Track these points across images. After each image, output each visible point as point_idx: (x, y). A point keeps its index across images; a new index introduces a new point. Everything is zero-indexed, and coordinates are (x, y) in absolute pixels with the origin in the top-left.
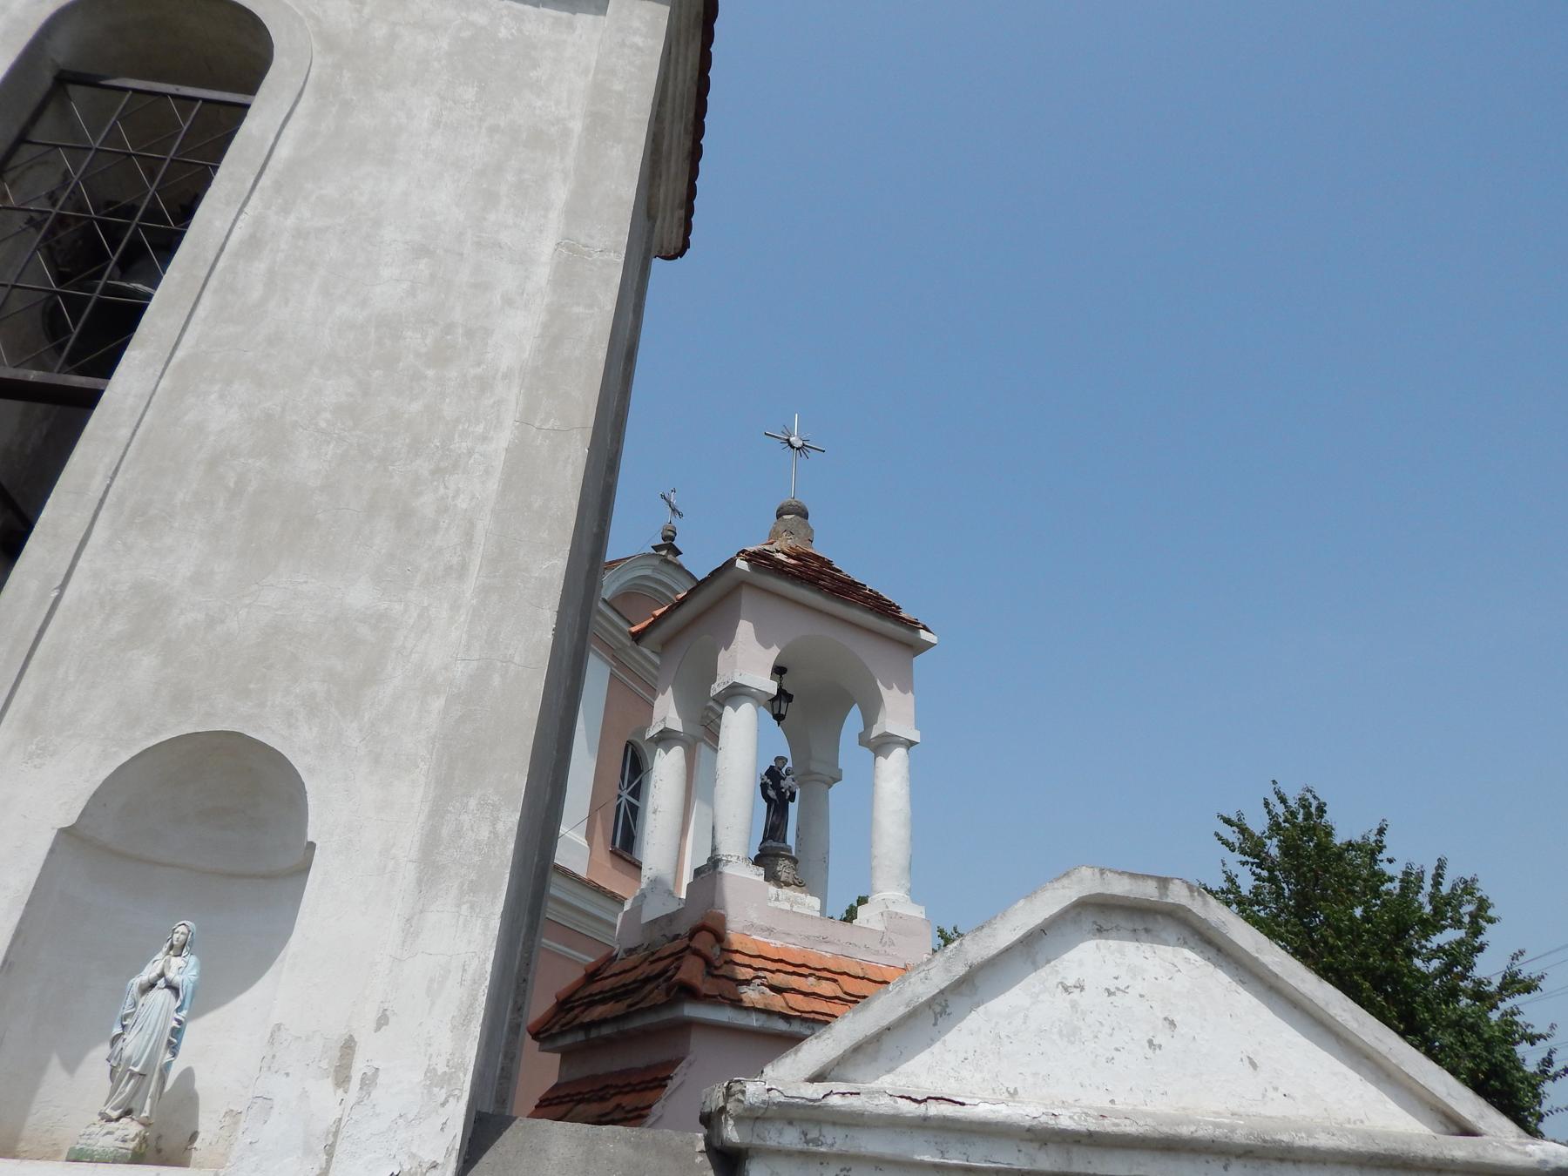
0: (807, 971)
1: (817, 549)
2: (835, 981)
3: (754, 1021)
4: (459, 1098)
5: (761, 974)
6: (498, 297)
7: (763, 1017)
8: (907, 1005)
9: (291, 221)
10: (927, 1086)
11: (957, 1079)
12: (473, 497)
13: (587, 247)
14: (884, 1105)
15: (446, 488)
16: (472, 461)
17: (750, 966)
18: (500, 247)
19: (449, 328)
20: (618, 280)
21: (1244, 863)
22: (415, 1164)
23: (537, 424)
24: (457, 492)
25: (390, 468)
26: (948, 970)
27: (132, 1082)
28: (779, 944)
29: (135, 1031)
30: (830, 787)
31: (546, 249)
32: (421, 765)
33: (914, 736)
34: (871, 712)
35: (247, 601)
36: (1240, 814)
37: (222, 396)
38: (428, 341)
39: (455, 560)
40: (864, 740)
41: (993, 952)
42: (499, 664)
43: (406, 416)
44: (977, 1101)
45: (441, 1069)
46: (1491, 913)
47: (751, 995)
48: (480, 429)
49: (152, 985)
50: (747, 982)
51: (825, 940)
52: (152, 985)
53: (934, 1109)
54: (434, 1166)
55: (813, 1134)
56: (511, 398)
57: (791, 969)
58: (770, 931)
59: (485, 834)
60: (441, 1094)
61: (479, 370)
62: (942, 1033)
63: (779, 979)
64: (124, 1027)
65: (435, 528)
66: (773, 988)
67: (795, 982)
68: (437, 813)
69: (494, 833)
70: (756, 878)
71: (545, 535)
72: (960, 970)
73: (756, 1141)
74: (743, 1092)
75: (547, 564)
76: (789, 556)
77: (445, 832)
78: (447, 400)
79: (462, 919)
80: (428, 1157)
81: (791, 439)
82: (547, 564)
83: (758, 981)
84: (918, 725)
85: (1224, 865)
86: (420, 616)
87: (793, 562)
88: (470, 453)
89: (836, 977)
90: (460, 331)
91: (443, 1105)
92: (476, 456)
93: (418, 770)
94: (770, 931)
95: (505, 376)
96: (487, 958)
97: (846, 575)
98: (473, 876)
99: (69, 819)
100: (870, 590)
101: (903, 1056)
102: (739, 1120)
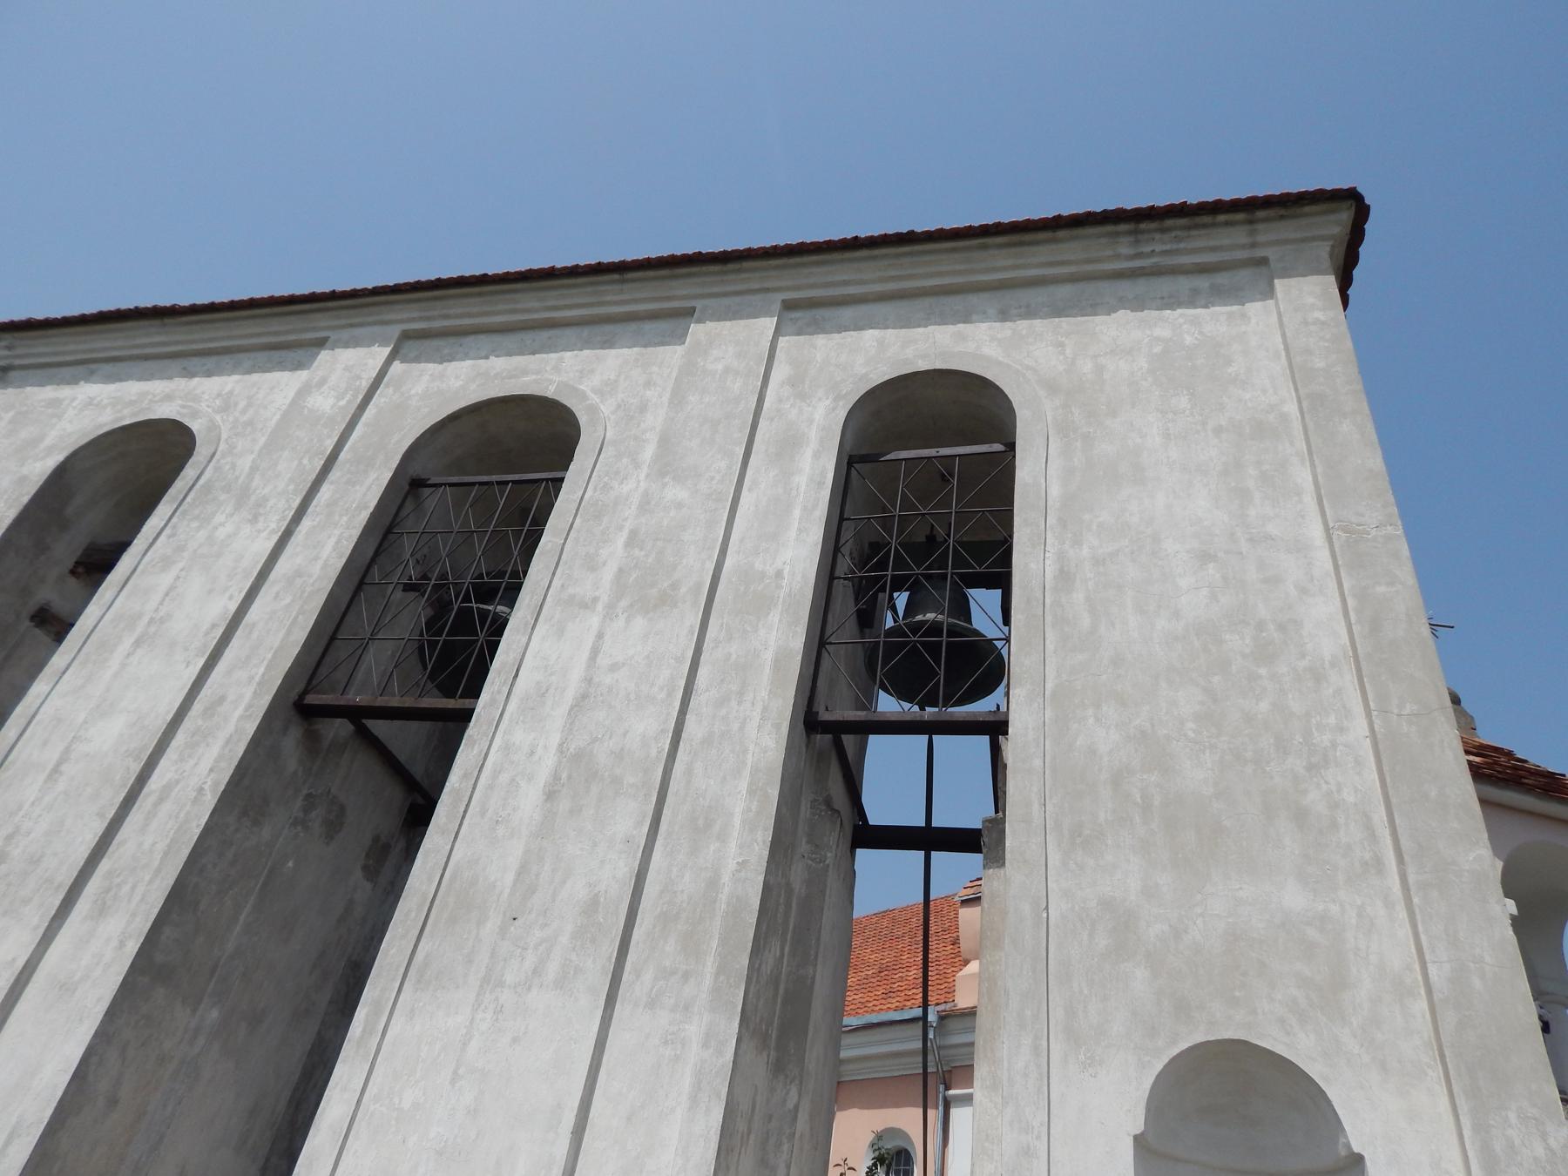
9: (1085, 551)
15: (1327, 783)
16: (1338, 754)
19: (1261, 626)
23: (1396, 711)
32: (1430, 1072)
35: (1199, 910)
37: (1097, 720)
38: (1247, 641)
39: (1367, 856)
42: (1472, 965)
48: (1332, 720)
59: (1540, 1151)
69: (1548, 1148)
77: (1498, 1146)
78: (1290, 696)
88: (1334, 745)
95: (1333, 665)
99: (1138, 1126)
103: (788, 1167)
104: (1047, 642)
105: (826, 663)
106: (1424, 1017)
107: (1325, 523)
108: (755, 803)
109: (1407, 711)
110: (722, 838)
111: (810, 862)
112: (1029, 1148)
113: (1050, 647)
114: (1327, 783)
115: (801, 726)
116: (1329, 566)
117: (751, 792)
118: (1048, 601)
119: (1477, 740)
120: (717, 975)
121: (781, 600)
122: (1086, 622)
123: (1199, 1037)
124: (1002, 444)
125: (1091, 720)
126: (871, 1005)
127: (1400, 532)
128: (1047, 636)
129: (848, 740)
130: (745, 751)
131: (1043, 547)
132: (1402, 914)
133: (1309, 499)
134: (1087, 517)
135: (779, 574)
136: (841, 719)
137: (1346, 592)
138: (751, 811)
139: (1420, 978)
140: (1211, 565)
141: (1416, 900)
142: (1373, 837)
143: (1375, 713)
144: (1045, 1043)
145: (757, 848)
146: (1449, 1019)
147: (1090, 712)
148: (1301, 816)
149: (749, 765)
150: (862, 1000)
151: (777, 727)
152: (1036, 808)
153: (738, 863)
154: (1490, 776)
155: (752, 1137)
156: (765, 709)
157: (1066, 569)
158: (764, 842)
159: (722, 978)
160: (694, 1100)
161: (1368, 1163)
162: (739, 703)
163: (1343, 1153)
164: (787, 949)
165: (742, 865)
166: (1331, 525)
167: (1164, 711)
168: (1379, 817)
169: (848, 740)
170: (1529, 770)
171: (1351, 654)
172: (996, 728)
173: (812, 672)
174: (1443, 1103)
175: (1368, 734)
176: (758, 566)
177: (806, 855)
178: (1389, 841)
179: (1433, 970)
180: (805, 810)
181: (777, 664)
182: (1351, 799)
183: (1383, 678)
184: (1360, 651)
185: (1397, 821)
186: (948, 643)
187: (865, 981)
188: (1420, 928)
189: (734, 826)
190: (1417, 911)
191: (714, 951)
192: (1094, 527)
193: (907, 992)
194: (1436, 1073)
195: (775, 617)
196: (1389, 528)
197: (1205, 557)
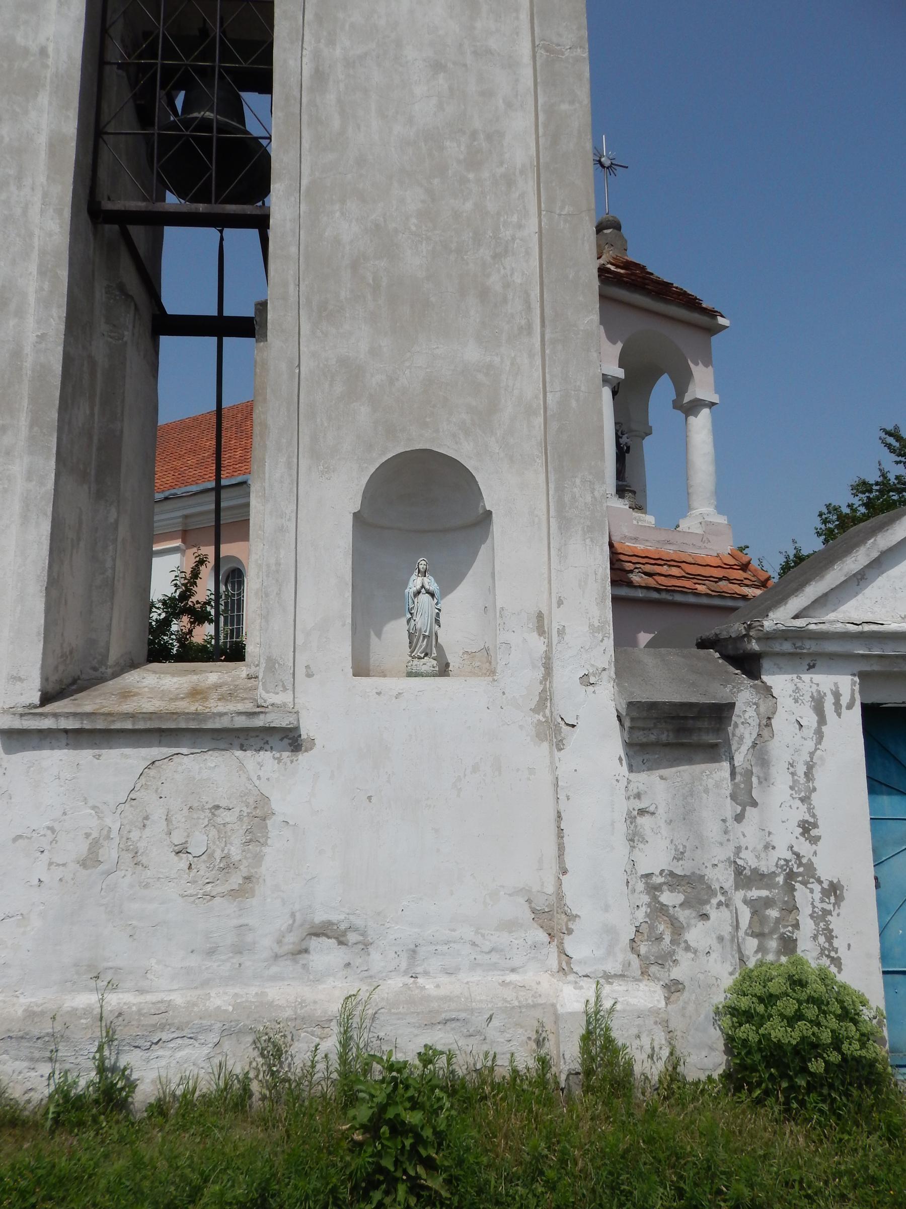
0: (663, 562)
1: (632, 256)
2: (679, 567)
3: (640, 594)
4: (609, 638)
5: (638, 566)
6: (501, 101)
7: (645, 591)
8: (846, 576)
9: (338, 52)
10: (857, 617)
11: (872, 613)
12: (523, 274)
13: (559, 45)
14: (839, 627)
15: (504, 268)
16: (515, 246)
17: (630, 562)
18: (491, 53)
19: (474, 135)
20: (587, 75)
21: (897, 463)
22: (595, 669)
23: (558, 212)
24: (513, 270)
25: (465, 257)
26: (868, 555)
27: (426, 640)
28: (642, 547)
29: (419, 616)
30: (643, 439)
31: (524, 49)
32: (537, 460)
33: (715, 398)
34: (682, 381)
35: (407, 364)
36: (896, 428)
37: (342, 214)
38: (463, 148)
39: (523, 322)
40: (678, 405)
41: (894, 543)
42: (573, 393)
43: (465, 214)
44: (890, 623)
45: (596, 624)
46: (886, 470)
47: (636, 578)
48: (515, 219)
49: (419, 592)
50: (631, 571)
51: (669, 543)
52: (419, 592)
53: (867, 628)
54: (604, 669)
55: (799, 644)
56: (527, 186)
57: (654, 562)
58: (636, 539)
59: (589, 499)
60: (600, 636)
61: (502, 170)
62: (862, 589)
63: (648, 568)
64: (411, 614)
65: (505, 300)
66: (646, 574)
67: (657, 569)
68: (559, 489)
69: (594, 497)
70: (624, 507)
71: (581, 298)
72: (875, 554)
73: (768, 649)
74: (762, 626)
75: (587, 319)
76: (617, 266)
77: (567, 499)
78: (488, 197)
79: (588, 548)
80: (601, 666)
81: (603, 160)
82: (587, 319)
83: (637, 570)
84: (717, 391)
85: (880, 465)
86: (512, 364)
87: (622, 271)
88: (513, 239)
89: (679, 564)
90: (482, 136)
91: (602, 641)
92: (518, 241)
93: (536, 464)
94: (636, 539)
95: (522, 172)
96: (607, 567)
97: (657, 277)
98: (588, 523)
99: (357, 507)
100: (677, 288)
101: (841, 602)
102: (758, 639)
103: (114, 560)
104: (303, 141)
105: (106, 156)
106: (540, 427)
107: (533, 41)
108: (47, 283)
109: (564, 212)
110: (20, 313)
111: (110, 340)
112: (283, 526)
113: (306, 145)
114: (504, 268)
115: (85, 215)
116: (530, 83)
117: (42, 273)
118: (304, 100)
119: (626, 258)
120: (31, 427)
121: (48, 80)
122: (336, 123)
123: (400, 450)
124: (808, 556)
125: (338, 214)
126: (207, 476)
127: (586, 55)
128: (303, 134)
129: (137, 232)
130: (31, 235)
131: (300, 43)
132: (538, 362)
133: (524, 16)
134: (341, 15)
135: (43, 52)
136: (123, 209)
137: (539, 108)
138: (43, 290)
139: (542, 403)
140: (442, 75)
141: (547, 351)
142: (529, 308)
143: (544, 213)
144: (296, 460)
145: (53, 323)
146: (554, 426)
147: (337, 207)
148: (484, 294)
149: (37, 248)
150: (200, 474)
151: (59, 212)
152: (292, 288)
153: (37, 336)
154: (627, 282)
155: (82, 544)
156: (45, 195)
157: (321, 68)
158: (59, 317)
159: (36, 429)
160: (25, 518)
161: (494, 515)
162: (19, 187)
163: (481, 511)
164: (96, 410)
165: (42, 337)
166: (537, 43)
167: (395, 207)
168: (535, 293)
169: (137, 232)
170: (652, 280)
171: (535, 164)
172: (261, 223)
173: (90, 161)
174: (543, 477)
175: (537, 230)
176: (20, 40)
177: (105, 333)
178: (538, 312)
179: (549, 396)
180: (99, 294)
181: (53, 148)
182: (519, 281)
183: (554, 184)
184: (541, 161)
185: (545, 296)
186: (218, 139)
187: (202, 461)
188: (547, 371)
189: (29, 305)
190: (547, 358)
191: (25, 409)
192: (347, 27)
193: (235, 466)
194: (540, 461)
195: (44, 99)
196: (579, 50)
197: (437, 67)
